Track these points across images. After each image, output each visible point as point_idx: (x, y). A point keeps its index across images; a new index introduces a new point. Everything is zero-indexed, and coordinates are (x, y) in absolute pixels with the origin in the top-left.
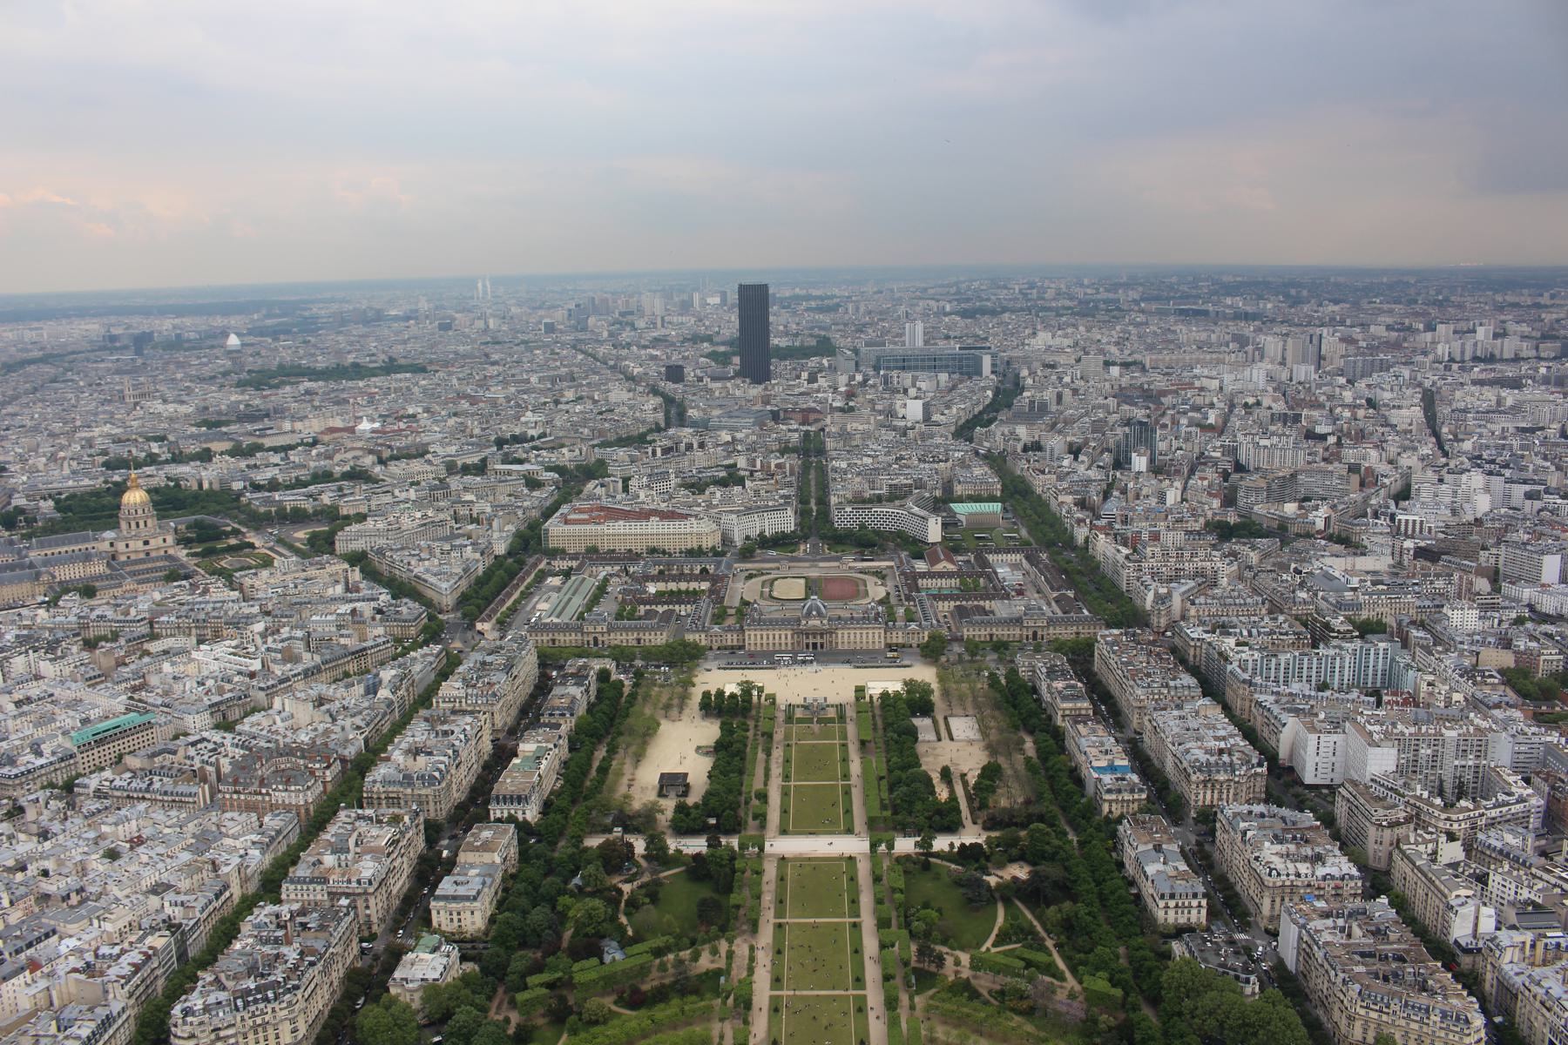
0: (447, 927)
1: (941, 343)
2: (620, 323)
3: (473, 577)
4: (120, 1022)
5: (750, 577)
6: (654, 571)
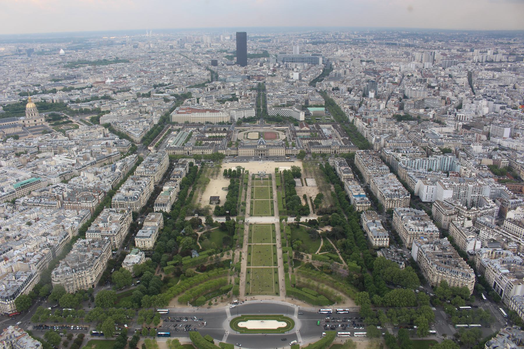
0: (141, 246)
1: (306, 53)
2: (196, 46)
3: (147, 132)
4: (35, 276)
5: (240, 132)
6: (208, 129)
